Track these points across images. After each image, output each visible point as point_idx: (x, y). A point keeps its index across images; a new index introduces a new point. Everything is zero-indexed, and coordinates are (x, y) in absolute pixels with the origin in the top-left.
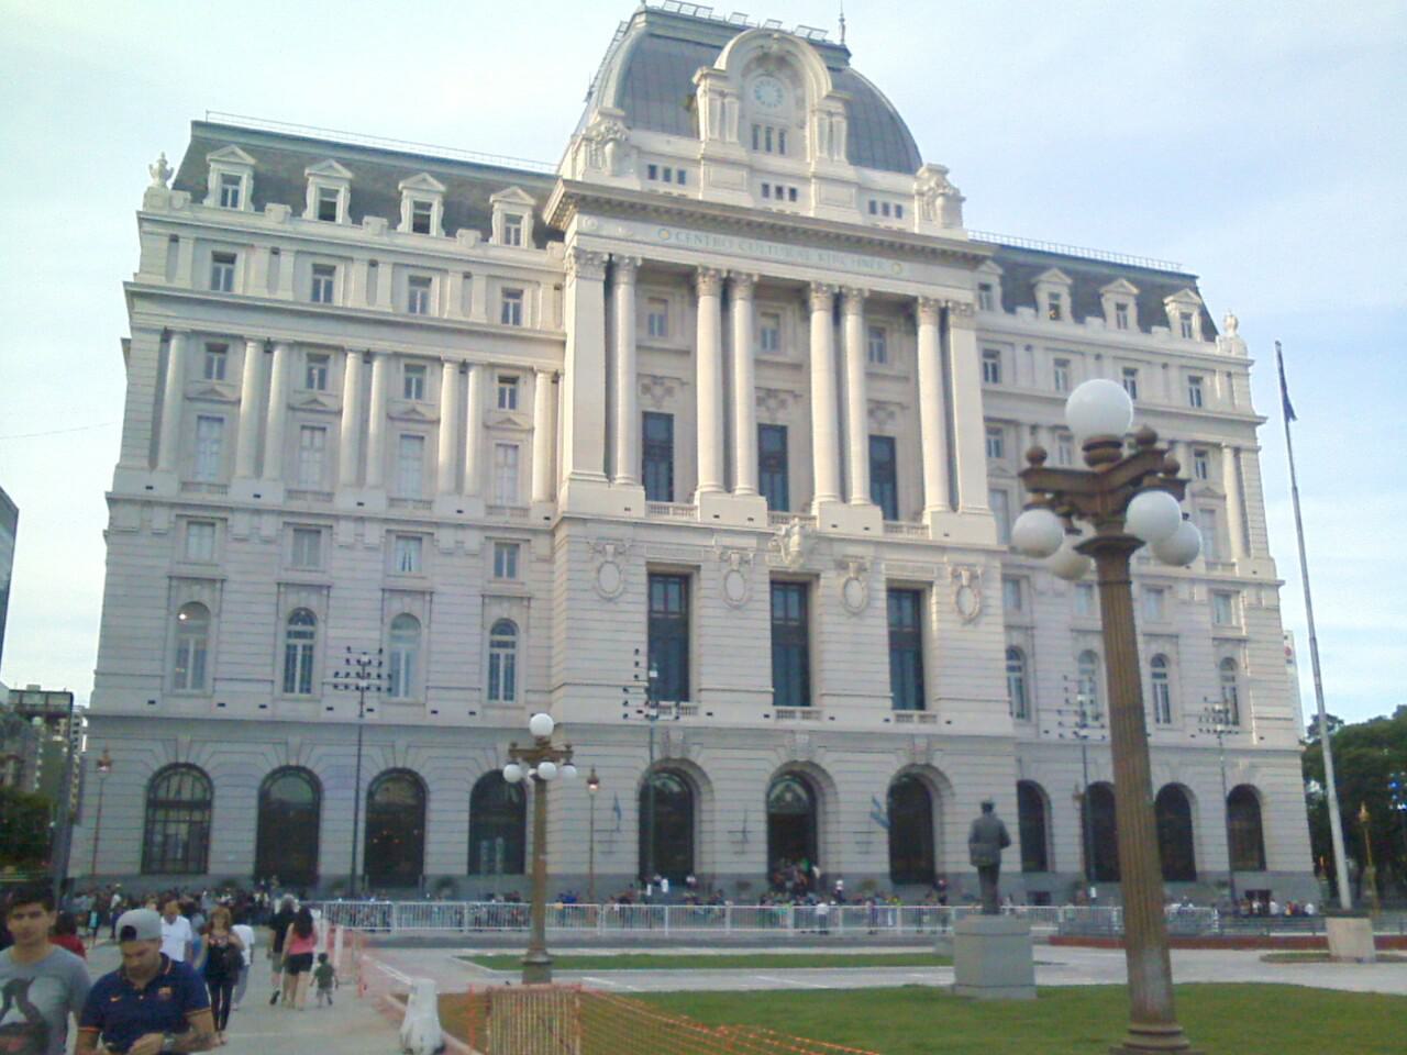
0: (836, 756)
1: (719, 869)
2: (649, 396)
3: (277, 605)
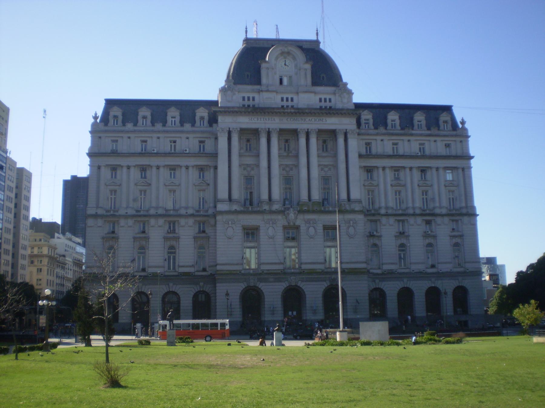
0: (263, 284)
1: (308, 318)
2: (246, 171)
3: (164, 244)
